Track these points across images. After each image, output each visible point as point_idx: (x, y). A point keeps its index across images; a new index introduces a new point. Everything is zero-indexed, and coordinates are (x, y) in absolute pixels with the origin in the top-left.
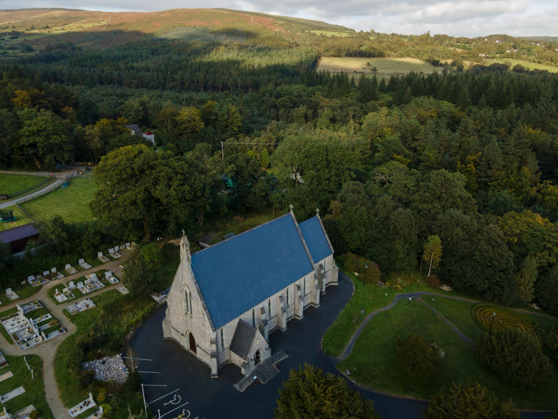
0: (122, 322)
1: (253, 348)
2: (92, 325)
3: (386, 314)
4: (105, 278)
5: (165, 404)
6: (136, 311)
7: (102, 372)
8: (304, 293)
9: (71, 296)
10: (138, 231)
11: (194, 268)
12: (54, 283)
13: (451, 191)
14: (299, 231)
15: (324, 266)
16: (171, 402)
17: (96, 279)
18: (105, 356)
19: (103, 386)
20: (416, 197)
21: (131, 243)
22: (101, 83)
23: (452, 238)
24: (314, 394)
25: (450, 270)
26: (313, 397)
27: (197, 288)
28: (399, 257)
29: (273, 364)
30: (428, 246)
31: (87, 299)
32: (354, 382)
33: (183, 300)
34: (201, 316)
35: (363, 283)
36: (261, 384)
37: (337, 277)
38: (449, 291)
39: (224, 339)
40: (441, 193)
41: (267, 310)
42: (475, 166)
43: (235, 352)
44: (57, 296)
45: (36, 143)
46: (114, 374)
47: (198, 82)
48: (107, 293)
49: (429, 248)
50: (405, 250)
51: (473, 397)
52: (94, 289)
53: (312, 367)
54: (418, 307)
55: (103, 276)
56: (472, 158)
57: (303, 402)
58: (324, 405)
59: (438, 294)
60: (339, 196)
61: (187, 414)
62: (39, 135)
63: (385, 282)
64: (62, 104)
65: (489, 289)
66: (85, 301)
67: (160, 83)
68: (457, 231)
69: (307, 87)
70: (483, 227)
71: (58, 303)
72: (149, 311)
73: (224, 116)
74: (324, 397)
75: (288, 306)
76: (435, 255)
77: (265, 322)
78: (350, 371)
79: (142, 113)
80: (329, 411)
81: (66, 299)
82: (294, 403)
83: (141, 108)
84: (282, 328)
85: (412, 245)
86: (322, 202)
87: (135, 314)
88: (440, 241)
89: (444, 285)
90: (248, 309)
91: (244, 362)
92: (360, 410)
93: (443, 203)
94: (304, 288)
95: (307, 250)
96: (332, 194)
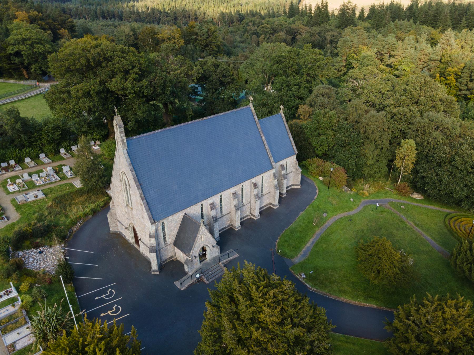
0: (70, 213)
1: (197, 244)
2: (36, 215)
3: (350, 219)
4: (62, 172)
5: (96, 298)
6: (87, 204)
7: (36, 261)
8: (262, 192)
9: (24, 186)
10: (102, 130)
11: (130, 154)
12: (11, 174)
13: (431, 94)
14: (259, 126)
15: (285, 167)
16: (103, 296)
17: (52, 173)
18: (45, 246)
19: (31, 276)
20: (391, 101)
21: (95, 142)
22: (104, 17)
23: (428, 143)
24: (251, 299)
25: (423, 177)
26: (248, 302)
27: (133, 176)
28: (368, 163)
29: (220, 263)
30: (400, 152)
31: (39, 190)
32: (309, 286)
33: (123, 190)
34: (140, 207)
35: (327, 188)
36: (205, 283)
37: (300, 180)
38: (420, 200)
39: (166, 233)
40: (420, 96)
41: (218, 206)
42: (456, 79)
43: (178, 248)
44: (9, 186)
45: (21, 51)
46: (48, 264)
47: (189, 17)
48: (60, 186)
49: (402, 152)
50: (375, 156)
51: (455, 312)
52: (48, 182)
53: (253, 266)
54: (385, 214)
55: (61, 170)
56: (453, 70)
57: (237, 307)
58: (262, 311)
59: (407, 201)
60: (308, 100)
61: (117, 309)
62: (23, 44)
63: (351, 188)
64: (59, 27)
65: (467, 197)
66: (36, 192)
67: (156, 18)
68: (436, 135)
69: (288, 19)
70: (466, 132)
71: (9, 193)
72: (101, 206)
73: (203, 35)
74: (263, 302)
75: (243, 205)
76: (408, 160)
77: (216, 219)
78: (305, 274)
79: (133, 37)
80: (268, 320)
81: (17, 189)
82: (225, 308)
83: (132, 33)
84: (235, 227)
85: (383, 151)
86: (291, 108)
87: (86, 207)
88: (415, 145)
89: (415, 193)
90: (195, 203)
91: (187, 259)
92: (307, 320)
93: (421, 107)
94: (262, 188)
95: (267, 147)
96: (301, 99)
